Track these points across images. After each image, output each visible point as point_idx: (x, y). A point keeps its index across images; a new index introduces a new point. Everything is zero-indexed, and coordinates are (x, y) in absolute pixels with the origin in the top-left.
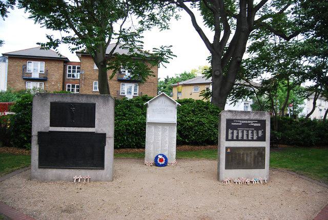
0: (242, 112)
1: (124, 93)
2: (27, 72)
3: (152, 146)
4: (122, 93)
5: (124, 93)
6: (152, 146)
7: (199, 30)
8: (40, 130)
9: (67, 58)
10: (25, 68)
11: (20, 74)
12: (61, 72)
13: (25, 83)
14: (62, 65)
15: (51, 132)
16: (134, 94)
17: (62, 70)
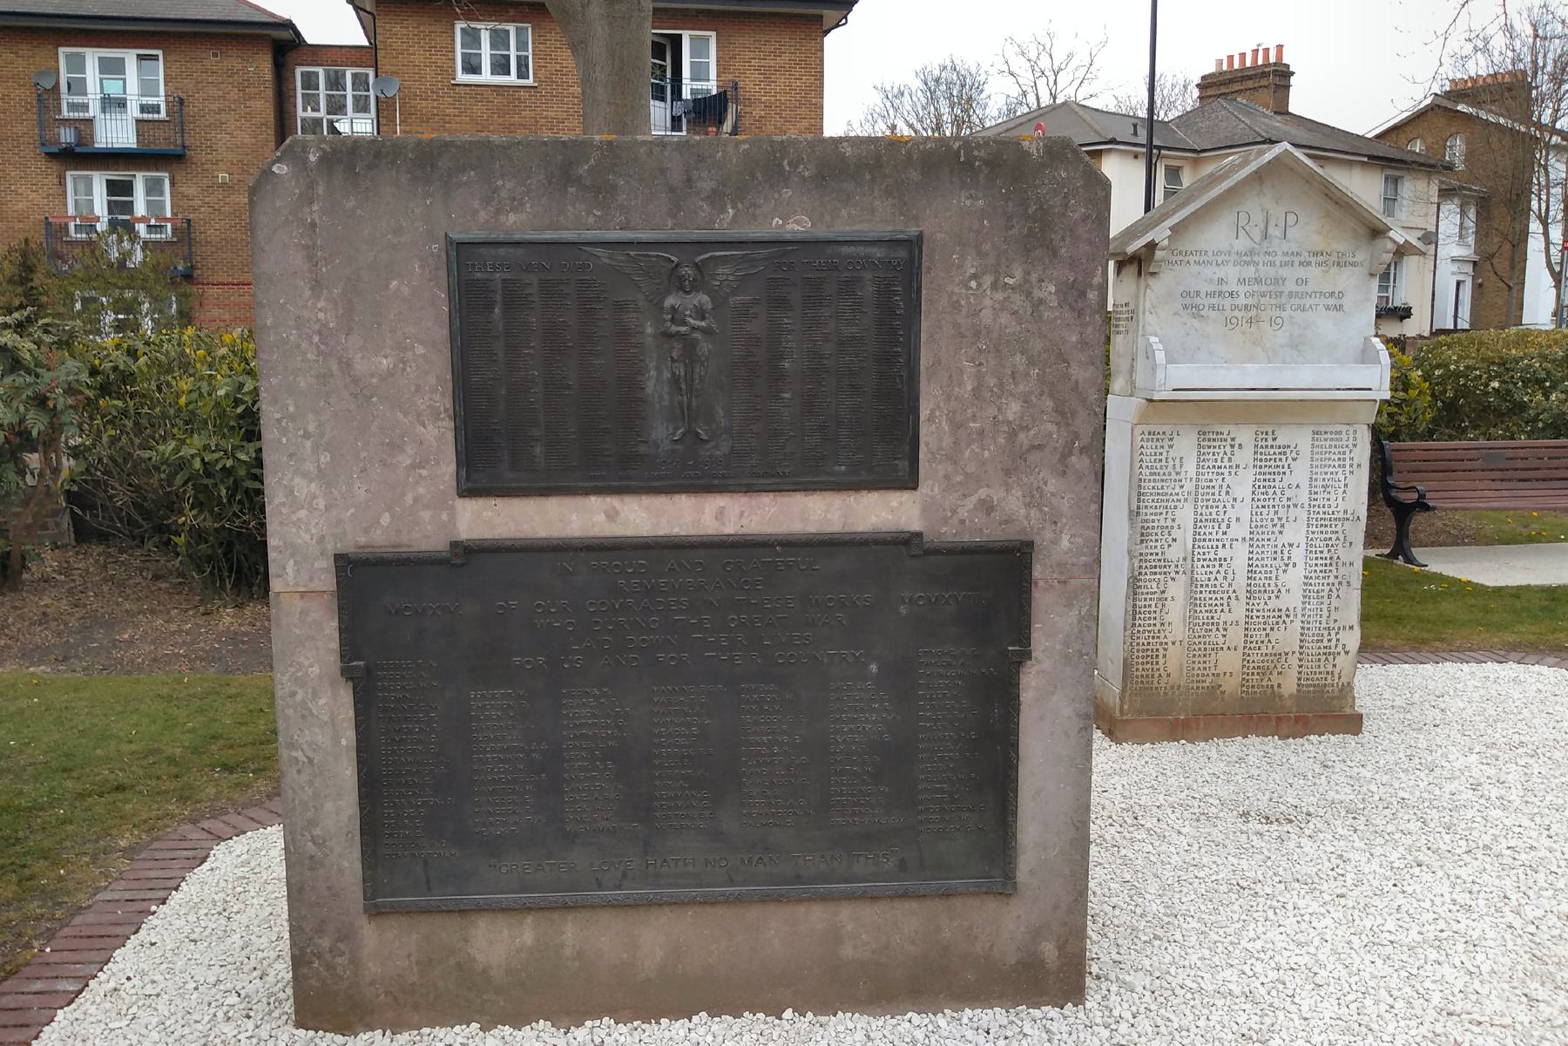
0: (1028, 113)
1: (85, 107)
2: (65, 113)
3: (1177, 590)
4: (73, 107)
5: (85, 107)
6: (1177, 590)
7: (1395, 274)
8: (355, 540)
9: (289, 25)
10: (48, 98)
11: (26, 127)
12: (264, 107)
13: (62, 183)
14: (262, 66)
15: (468, 554)
16: (143, 109)
17: (270, 93)
